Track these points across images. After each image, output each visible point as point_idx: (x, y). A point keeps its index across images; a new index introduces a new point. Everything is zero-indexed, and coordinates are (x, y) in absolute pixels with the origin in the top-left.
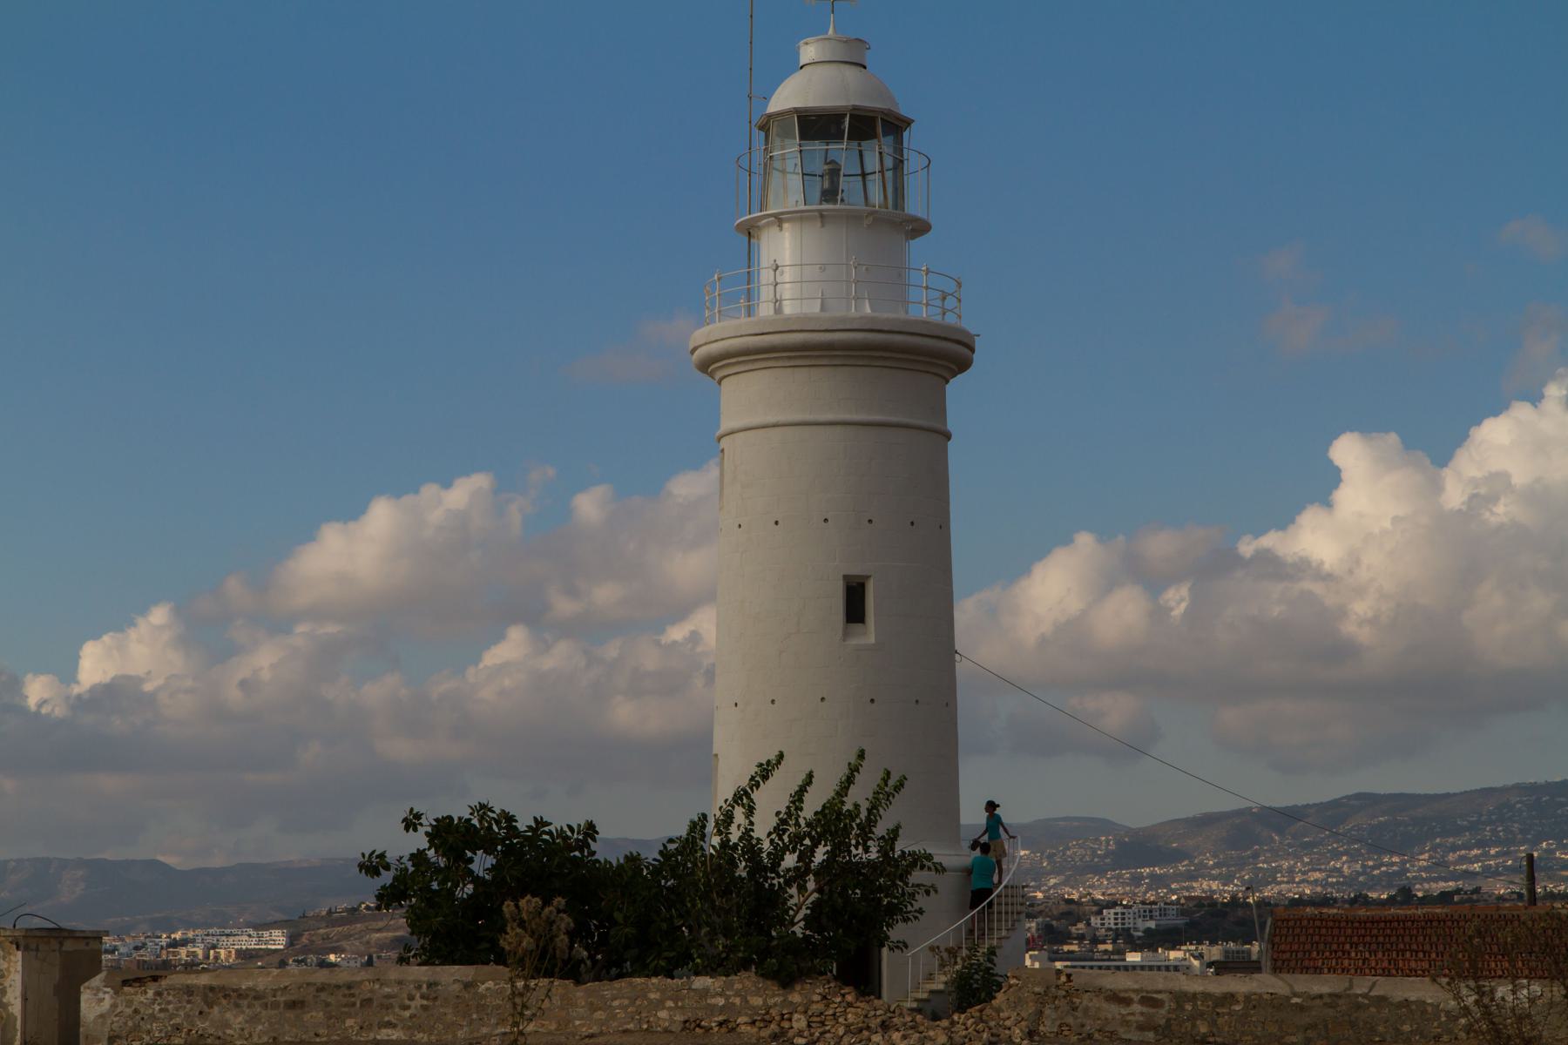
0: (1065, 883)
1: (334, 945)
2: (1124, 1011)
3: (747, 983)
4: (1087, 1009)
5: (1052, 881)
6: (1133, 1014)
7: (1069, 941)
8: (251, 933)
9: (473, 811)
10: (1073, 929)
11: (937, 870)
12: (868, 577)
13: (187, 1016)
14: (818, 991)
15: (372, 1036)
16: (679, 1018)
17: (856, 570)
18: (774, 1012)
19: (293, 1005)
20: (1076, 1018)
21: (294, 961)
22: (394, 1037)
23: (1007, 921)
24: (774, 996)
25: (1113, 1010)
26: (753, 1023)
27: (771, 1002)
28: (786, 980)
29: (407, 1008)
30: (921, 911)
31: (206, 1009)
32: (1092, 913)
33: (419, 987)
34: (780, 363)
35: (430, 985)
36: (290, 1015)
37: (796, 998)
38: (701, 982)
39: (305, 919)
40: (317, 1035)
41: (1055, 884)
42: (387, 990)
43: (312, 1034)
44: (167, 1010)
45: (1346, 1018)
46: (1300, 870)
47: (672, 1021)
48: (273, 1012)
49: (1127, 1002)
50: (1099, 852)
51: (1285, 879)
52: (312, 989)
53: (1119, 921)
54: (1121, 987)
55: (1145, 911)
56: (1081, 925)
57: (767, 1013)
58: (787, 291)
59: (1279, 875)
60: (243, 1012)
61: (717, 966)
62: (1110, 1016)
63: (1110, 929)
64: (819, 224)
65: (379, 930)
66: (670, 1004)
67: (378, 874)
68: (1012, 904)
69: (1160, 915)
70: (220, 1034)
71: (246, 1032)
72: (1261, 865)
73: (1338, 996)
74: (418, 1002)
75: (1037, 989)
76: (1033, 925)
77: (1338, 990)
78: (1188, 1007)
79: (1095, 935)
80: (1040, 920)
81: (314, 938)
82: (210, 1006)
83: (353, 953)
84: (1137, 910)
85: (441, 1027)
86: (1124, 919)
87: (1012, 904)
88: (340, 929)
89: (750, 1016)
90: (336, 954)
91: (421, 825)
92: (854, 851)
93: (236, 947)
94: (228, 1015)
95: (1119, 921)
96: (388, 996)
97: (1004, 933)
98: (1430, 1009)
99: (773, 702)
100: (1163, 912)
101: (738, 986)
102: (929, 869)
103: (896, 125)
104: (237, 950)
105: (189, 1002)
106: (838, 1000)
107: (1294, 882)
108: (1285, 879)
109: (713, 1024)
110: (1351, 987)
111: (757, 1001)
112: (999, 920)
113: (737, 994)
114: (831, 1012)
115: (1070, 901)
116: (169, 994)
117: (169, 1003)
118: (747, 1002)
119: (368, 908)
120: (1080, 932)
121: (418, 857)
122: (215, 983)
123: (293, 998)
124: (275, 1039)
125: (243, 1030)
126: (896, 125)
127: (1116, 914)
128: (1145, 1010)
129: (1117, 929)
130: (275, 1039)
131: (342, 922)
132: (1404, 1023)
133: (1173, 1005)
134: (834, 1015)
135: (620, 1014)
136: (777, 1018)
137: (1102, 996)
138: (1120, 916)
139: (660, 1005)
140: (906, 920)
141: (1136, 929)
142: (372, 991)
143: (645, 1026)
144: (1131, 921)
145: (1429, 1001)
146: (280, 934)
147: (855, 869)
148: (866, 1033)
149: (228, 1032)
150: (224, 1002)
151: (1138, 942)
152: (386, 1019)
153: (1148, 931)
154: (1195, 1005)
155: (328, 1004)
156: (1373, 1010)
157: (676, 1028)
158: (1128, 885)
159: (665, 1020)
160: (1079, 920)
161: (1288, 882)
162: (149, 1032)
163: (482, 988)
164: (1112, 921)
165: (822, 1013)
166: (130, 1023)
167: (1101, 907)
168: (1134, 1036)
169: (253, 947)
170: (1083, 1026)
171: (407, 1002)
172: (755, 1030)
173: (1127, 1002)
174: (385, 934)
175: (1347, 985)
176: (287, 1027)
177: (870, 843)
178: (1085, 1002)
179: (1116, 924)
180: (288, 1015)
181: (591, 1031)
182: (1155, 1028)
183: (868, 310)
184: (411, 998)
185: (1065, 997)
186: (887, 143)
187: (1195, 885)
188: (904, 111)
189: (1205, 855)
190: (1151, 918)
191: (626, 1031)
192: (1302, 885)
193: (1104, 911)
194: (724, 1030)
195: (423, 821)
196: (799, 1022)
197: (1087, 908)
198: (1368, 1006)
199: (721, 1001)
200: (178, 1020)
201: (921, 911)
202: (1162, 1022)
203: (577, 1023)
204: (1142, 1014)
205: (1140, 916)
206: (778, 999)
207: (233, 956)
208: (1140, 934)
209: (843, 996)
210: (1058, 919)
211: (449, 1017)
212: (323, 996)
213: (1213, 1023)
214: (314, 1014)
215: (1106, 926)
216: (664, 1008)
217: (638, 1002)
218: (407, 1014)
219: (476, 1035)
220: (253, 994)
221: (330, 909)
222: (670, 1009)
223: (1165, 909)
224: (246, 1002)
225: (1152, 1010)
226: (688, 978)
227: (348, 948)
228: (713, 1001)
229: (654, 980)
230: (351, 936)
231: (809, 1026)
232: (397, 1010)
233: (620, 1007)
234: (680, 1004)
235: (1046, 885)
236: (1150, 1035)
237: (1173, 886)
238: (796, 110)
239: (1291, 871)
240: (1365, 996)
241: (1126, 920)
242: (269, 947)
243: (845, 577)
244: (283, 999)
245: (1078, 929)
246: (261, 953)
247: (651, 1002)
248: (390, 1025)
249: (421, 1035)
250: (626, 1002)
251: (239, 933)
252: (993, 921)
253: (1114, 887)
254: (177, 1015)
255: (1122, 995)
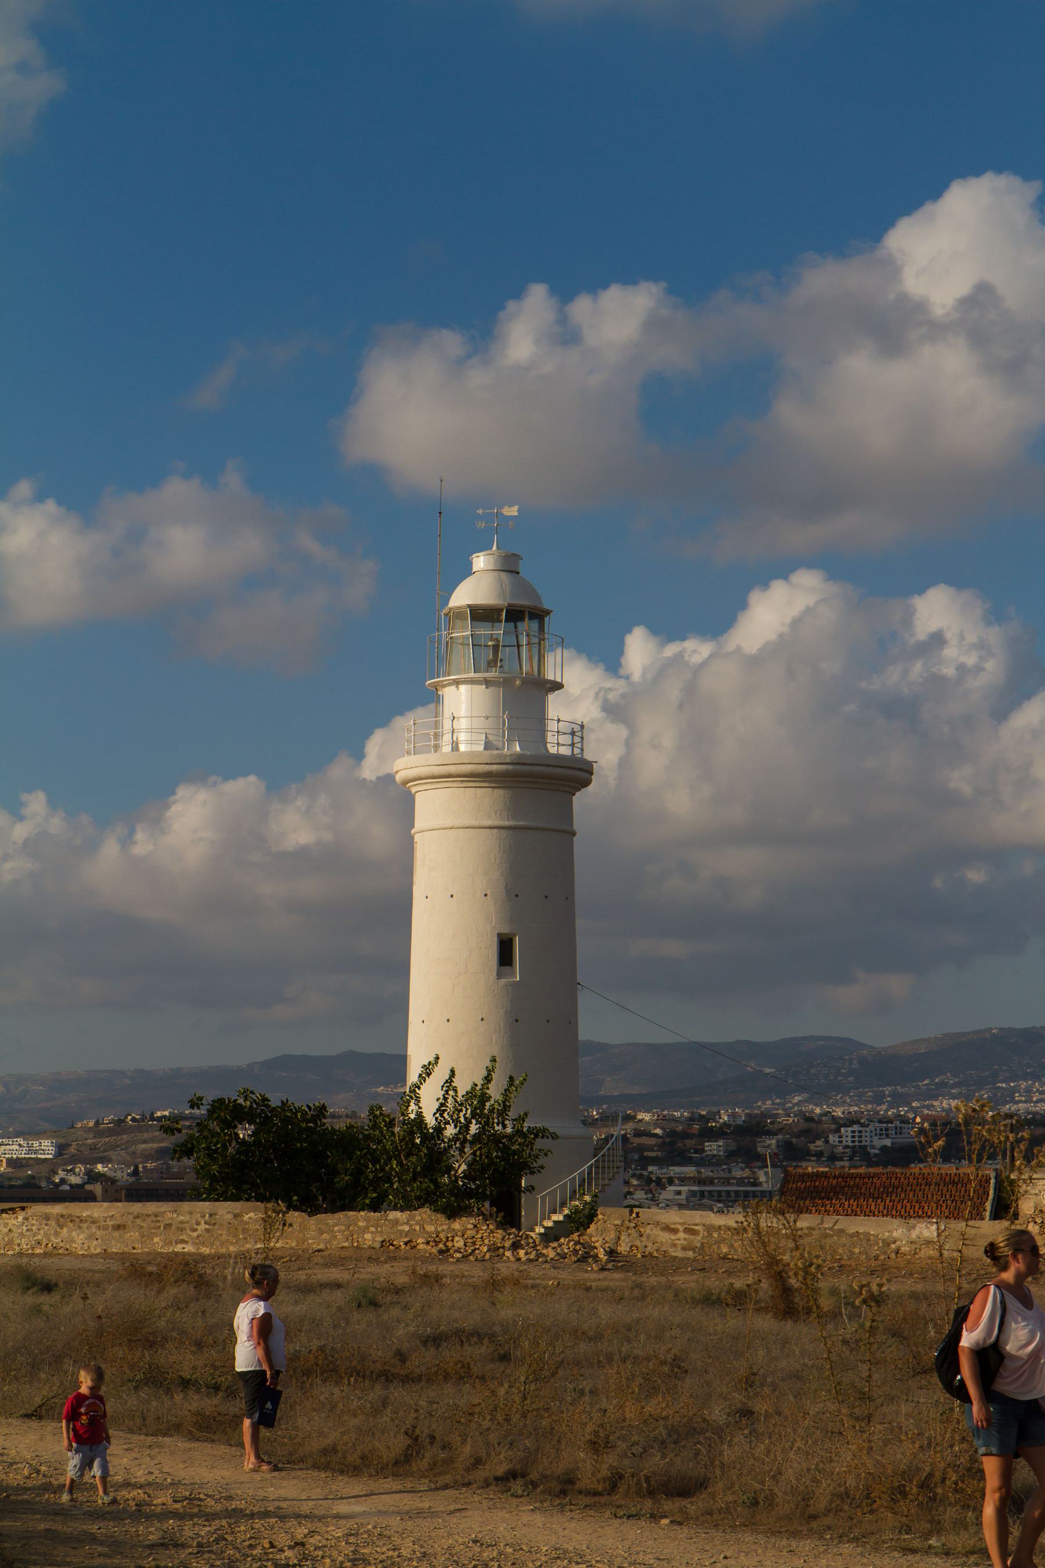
0: (808, 1101)
1: (101, 1155)
2: (673, 1237)
3: (424, 1216)
4: (648, 1236)
5: (797, 1099)
6: (679, 1239)
7: (808, 1158)
8: (22, 1142)
9: (240, 1094)
10: (812, 1147)
11: (553, 1138)
12: (515, 935)
13: (46, 1234)
14: (471, 1222)
15: (171, 1250)
16: (379, 1239)
17: (505, 930)
18: (442, 1235)
19: (118, 1227)
20: (641, 1241)
21: (63, 1170)
22: (186, 1250)
23: (609, 1173)
24: (442, 1225)
25: (665, 1237)
26: (428, 1243)
27: (440, 1229)
28: (452, 1213)
29: (195, 1230)
30: (542, 1167)
31: (58, 1230)
32: (831, 1131)
33: (204, 1216)
34: (455, 785)
35: (211, 1215)
36: (116, 1234)
37: (457, 1225)
38: (393, 1215)
39: (73, 1130)
40: (134, 1248)
41: (800, 1101)
42: (182, 1218)
43: (130, 1247)
44: (32, 1230)
45: (818, 1243)
46: (1038, 1090)
47: (374, 1241)
48: (105, 1232)
49: (675, 1231)
50: (843, 1071)
51: (1023, 1099)
52: (131, 1217)
53: (857, 1139)
54: (671, 1221)
55: (881, 1130)
56: (819, 1143)
57: (437, 1236)
58: (462, 737)
59: (1017, 1095)
60: (84, 1232)
61: (407, 1205)
62: (664, 1241)
63: (847, 1147)
64: (484, 686)
65: (145, 1142)
66: (372, 1229)
67: (173, 1134)
68: (613, 1161)
69: (896, 1133)
70: (68, 1246)
71: (86, 1245)
72: (1000, 1085)
73: (812, 1229)
74: (203, 1226)
75: (616, 1222)
76: (774, 1141)
77: (813, 1225)
78: (715, 1235)
79: (833, 1152)
80: (780, 1137)
81: (82, 1148)
82: (61, 1227)
83: (119, 1163)
84: (873, 1129)
85: (218, 1243)
86: (860, 1137)
87: (613, 1161)
88: (107, 1139)
89: (426, 1238)
90: (103, 1164)
91: (202, 1104)
92: (497, 1128)
93: (7, 1156)
94: (74, 1233)
95: (857, 1139)
96: (182, 1222)
97: (606, 1182)
98: (872, 1238)
99: (448, 1020)
100: (898, 1130)
101: (418, 1218)
102: (548, 1137)
103: (539, 615)
104: (8, 1160)
105: (47, 1225)
106: (485, 1228)
107: (1031, 1101)
108: (1023, 1099)
109: (402, 1244)
110: (822, 1222)
111: (430, 1228)
112: (603, 1173)
113: (418, 1223)
114: (479, 1236)
115: (810, 1120)
116: (33, 1219)
117: (33, 1225)
118: (424, 1228)
119: (134, 1120)
120: (819, 1149)
121: (201, 1125)
122: (64, 1213)
123: (118, 1223)
124: (105, 1250)
125: (83, 1244)
126: (539, 615)
127: (854, 1132)
128: (687, 1236)
129: (854, 1147)
130: (105, 1250)
131: (109, 1132)
132: (855, 1247)
133: (706, 1234)
134: (482, 1238)
135: (340, 1236)
136: (444, 1240)
137: (659, 1227)
138: (857, 1134)
139: (366, 1230)
140: (532, 1173)
141: (872, 1147)
142: (171, 1218)
143: (356, 1244)
144: (868, 1139)
145: (872, 1233)
146: (49, 1144)
147: (497, 1139)
148: (501, 1250)
149: (74, 1245)
150: (71, 1225)
151: (874, 1159)
152: (181, 1237)
153: (884, 1148)
154: (720, 1234)
155: (141, 1227)
156: (835, 1238)
157: (377, 1245)
158: (870, 1102)
159: (369, 1240)
160: (818, 1137)
161: (1025, 1102)
162: (19, 1245)
163: (246, 1217)
164: (850, 1139)
165: (473, 1237)
166: (6, 1239)
167: (839, 1124)
168: (680, 1254)
169: (23, 1156)
170: (646, 1247)
171: (195, 1227)
172: (429, 1247)
173: (675, 1231)
174: (150, 1145)
175: (819, 1221)
176: (114, 1242)
177: (507, 1122)
178: (648, 1231)
179: (853, 1142)
180: (114, 1234)
181: (319, 1247)
182: (693, 1249)
183: (518, 749)
184: (198, 1224)
185: (634, 1228)
186: (535, 625)
187: (935, 1103)
188: (546, 606)
189: (946, 1075)
190: (887, 1136)
191: (342, 1248)
192: (1039, 1105)
193: (842, 1129)
194: (408, 1248)
195: (204, 1101)
196: (459, 1243)
197: (826, 1126)
198: (831, 1236)
199: (406, 1228)
200: (39, 1237)
201: (542, 1167)
202: (698, 1245)
203: (310, 1241)
204: (685, 1239)
205: (876, 1135)
206: (445, 1227)
207: (4, 1165)
208: (877, 1151)
209: (488, 1225)
210: (798, 1136)
211: (224, 1236)
212: (138, 1221)
213: (732, 1246)
214: (132, 1234)
215: (844, 1143)
216: (368, 1232)
217: (351, 1228)
218: (195, 1234)
219: (242, 1249)
220: (90, 1220)
221: (98, 1121)
222: (372, 1233)
223: (901, 1128)
224: (85, 1225)
225: (692, 1237)
226: (385, 1212)
227: (114, 1158)
228: (400, 1228)
229: (362, 1213)
230: (118, 1146)
231: (465, 1245)
232: (189, 1231)
233: (339, 1231)
234: (379, 1229)
235: (790, 1102)
236: (690, 1254)
237: (914, 1105)
238: (469, 606)
239: (1029, 1091)
240: (831, 1229)
241: (863, 1138)
242: (39, 1156)
243: (499, 934)
244: (111, 1223)
245: (816, 1147)
246: (32, 1162)
247: (359, 1227)
248: (183, 1241)
249: (205, 1249)
250: (343, 1228)
251: (10, 1143)
252: (592, 1179)
253: (856, 1105)
254: (38, 1234)
255: (673, 1226)
